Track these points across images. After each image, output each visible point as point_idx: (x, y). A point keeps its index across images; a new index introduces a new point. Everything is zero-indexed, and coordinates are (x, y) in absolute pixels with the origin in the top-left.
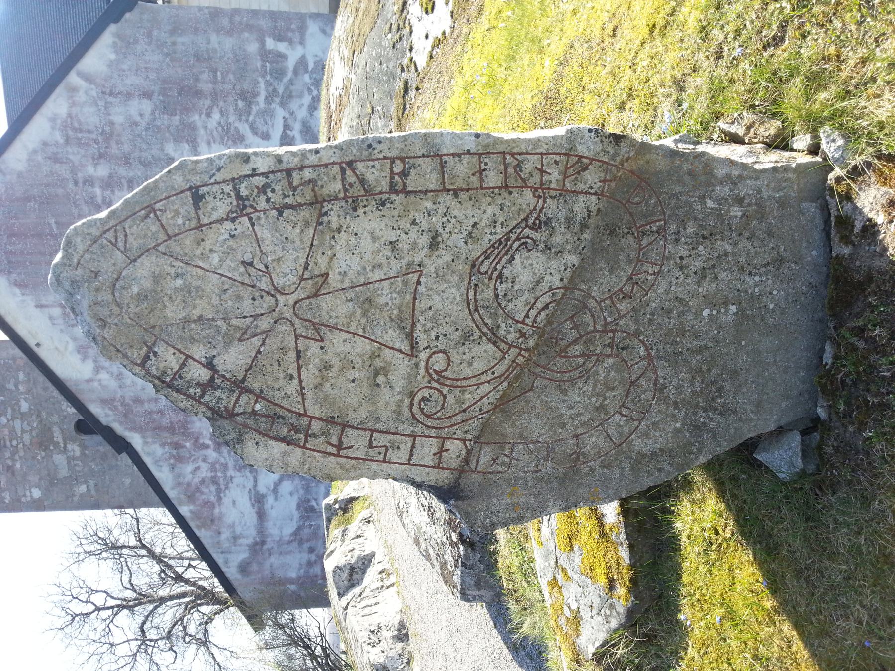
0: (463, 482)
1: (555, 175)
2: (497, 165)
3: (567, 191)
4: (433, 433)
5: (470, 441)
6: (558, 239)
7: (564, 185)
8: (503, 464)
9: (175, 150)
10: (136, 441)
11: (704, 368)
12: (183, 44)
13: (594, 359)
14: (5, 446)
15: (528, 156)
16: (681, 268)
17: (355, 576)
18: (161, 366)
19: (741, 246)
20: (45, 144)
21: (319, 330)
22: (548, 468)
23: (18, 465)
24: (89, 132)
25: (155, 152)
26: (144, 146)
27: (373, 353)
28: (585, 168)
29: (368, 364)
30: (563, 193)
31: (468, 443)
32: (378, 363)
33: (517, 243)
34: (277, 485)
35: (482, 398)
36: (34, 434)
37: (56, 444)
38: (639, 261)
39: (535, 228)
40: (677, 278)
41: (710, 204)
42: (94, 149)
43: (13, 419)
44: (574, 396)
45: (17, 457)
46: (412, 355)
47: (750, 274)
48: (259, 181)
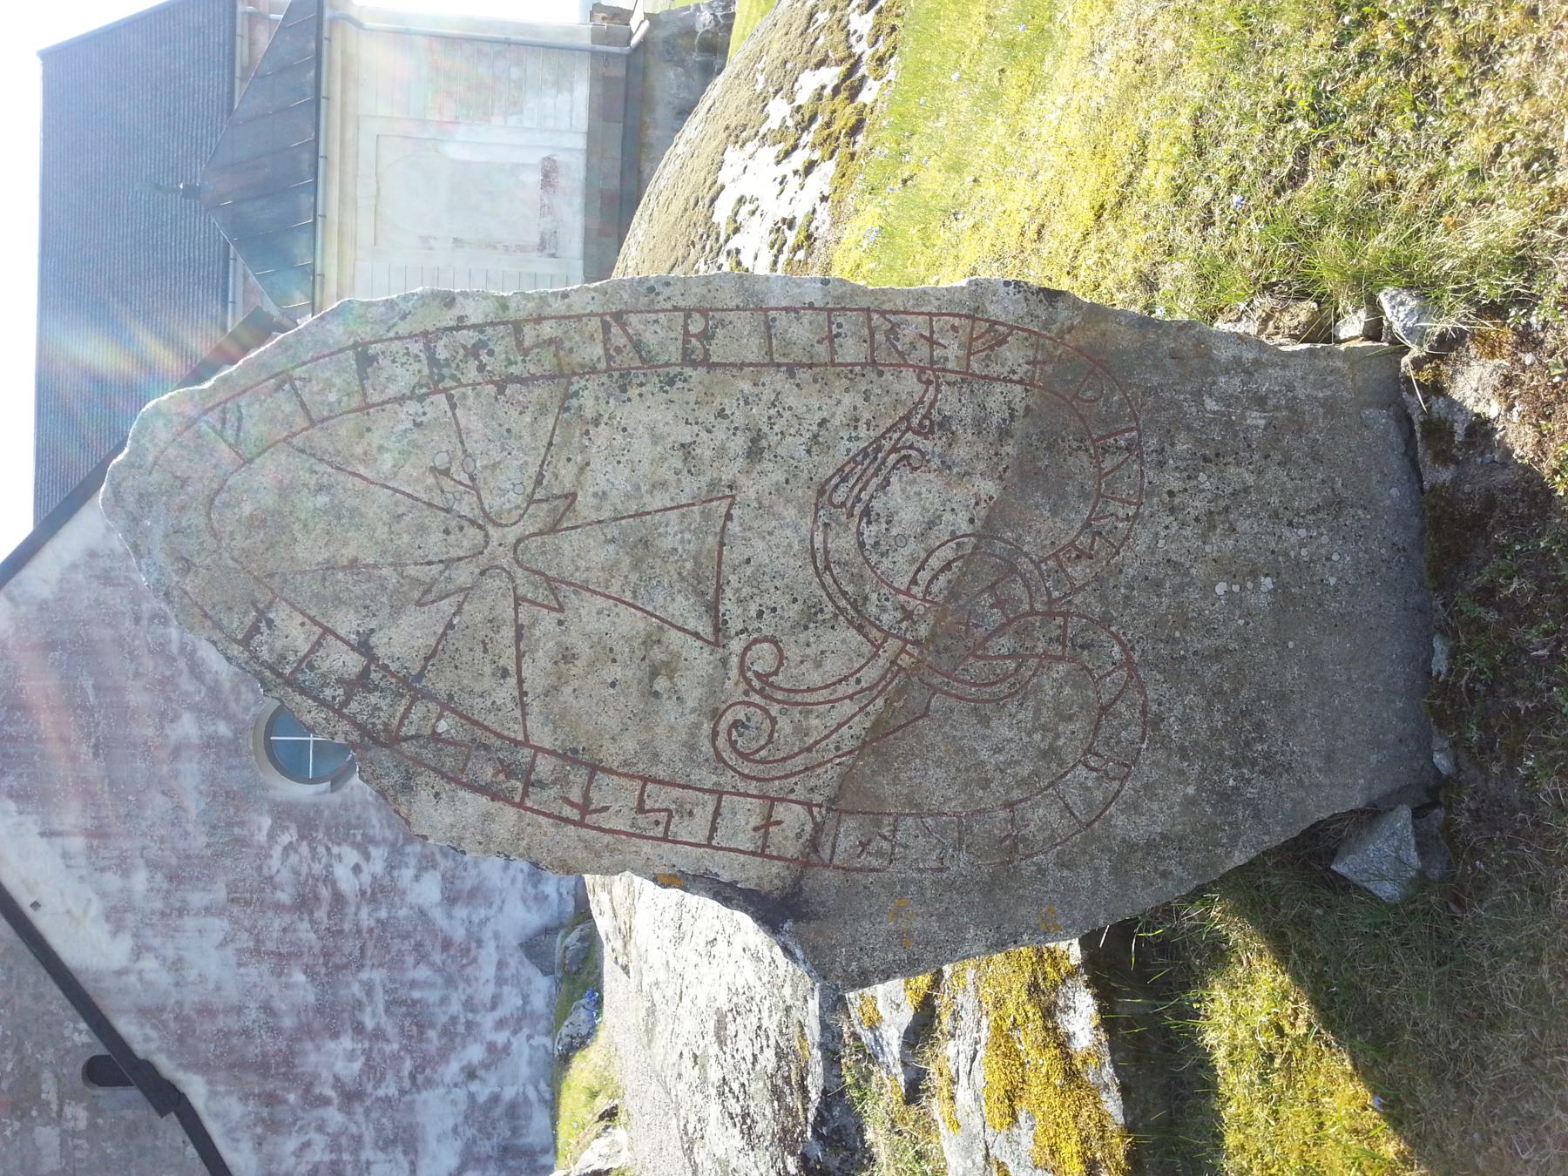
0: (808, 884)
1: (952, 351)
2: (865, 332)
3: (973, 375)
4: (753, 787)
5: (820, 806)
6: (961, 452)
7: (968, 365)
8: (879, 853)
10: (196, 1089)
15: (909, 317)
19: (1269, 476)
21: (556, 590)
27: (649, 636)
28: (1002, 341)
29: (639, 653)
31: (816, 810)
32: (658, 654)
35: (840, 726)
40: (1167, 527)
44: (1002, 729)
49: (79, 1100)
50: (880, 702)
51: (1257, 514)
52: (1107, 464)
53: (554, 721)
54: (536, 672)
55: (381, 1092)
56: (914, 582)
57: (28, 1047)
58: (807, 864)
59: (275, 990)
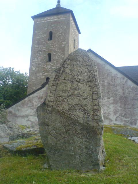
0: (46, 105)
1: (96, 118)
2: (97, 109)
4: (54, 100)
6: (85, 119)
9: (111, 99)
10: (44, 89)
11: (63, 149)
12: (136, 102)
13: (65, 127)
17: (10, 128)
20: (111, 73)
21: (72, 82)
22: (46, 120)
23: (40, 66)
24: (114, 82)
25: (111, 95)
26: (112, 93)
28: (97, 123)
30: (93, 120)
32: (66, 91)
34: (30, 121)
36: (47, 69)
37: (44, 73)
39: (87, 115)
41: (92, 147)
42: (110, 82)
44: (59, 124)
45: (42, 66)
47: (79, 156)
48: (93, 73)
50: (62, 112)
52: (85, 135)
53: (61, 83)
54: (64, 81)
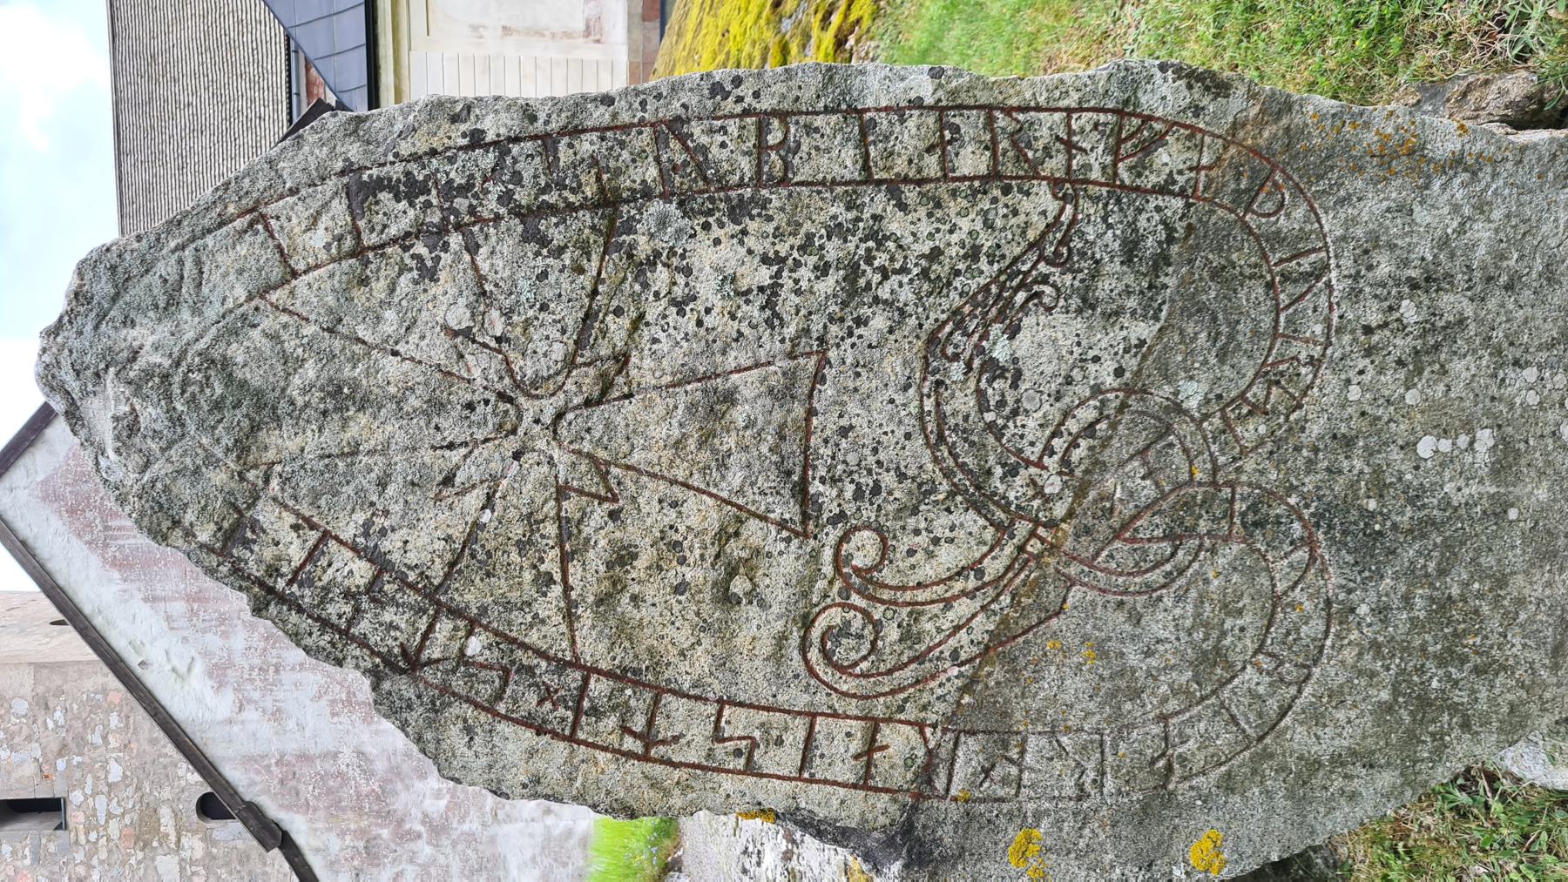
1: (1095, 160)
3: (1123, 186)
4: (853, 707)
5: (934, 726)
6: (1104, 287)
7: (1116, 174)
8: (1005, 781)
14: (77, 842)
15: (1042, 115)
16: (1369, 352)
18: (268, 554)
19: (1492, 304)
27: (722, 529)
29: (712, 551)
31: (928, 731)
32: (735, 549)
33: (1021, 297)
35: (957, 628)
36: (127, 820)
38: (1275, 335)
40: (1361, 372)
43: (95, 794)
45: (95, 862)
46: (805, 535)
49: (195, 832)
50: (1005, 599)
51: (1475, 351)
54: (587, 576)
55: (466, 827)
56: (1049, 450)
57: (147, 787)
58: (919, 796)
59: (365, 737)
